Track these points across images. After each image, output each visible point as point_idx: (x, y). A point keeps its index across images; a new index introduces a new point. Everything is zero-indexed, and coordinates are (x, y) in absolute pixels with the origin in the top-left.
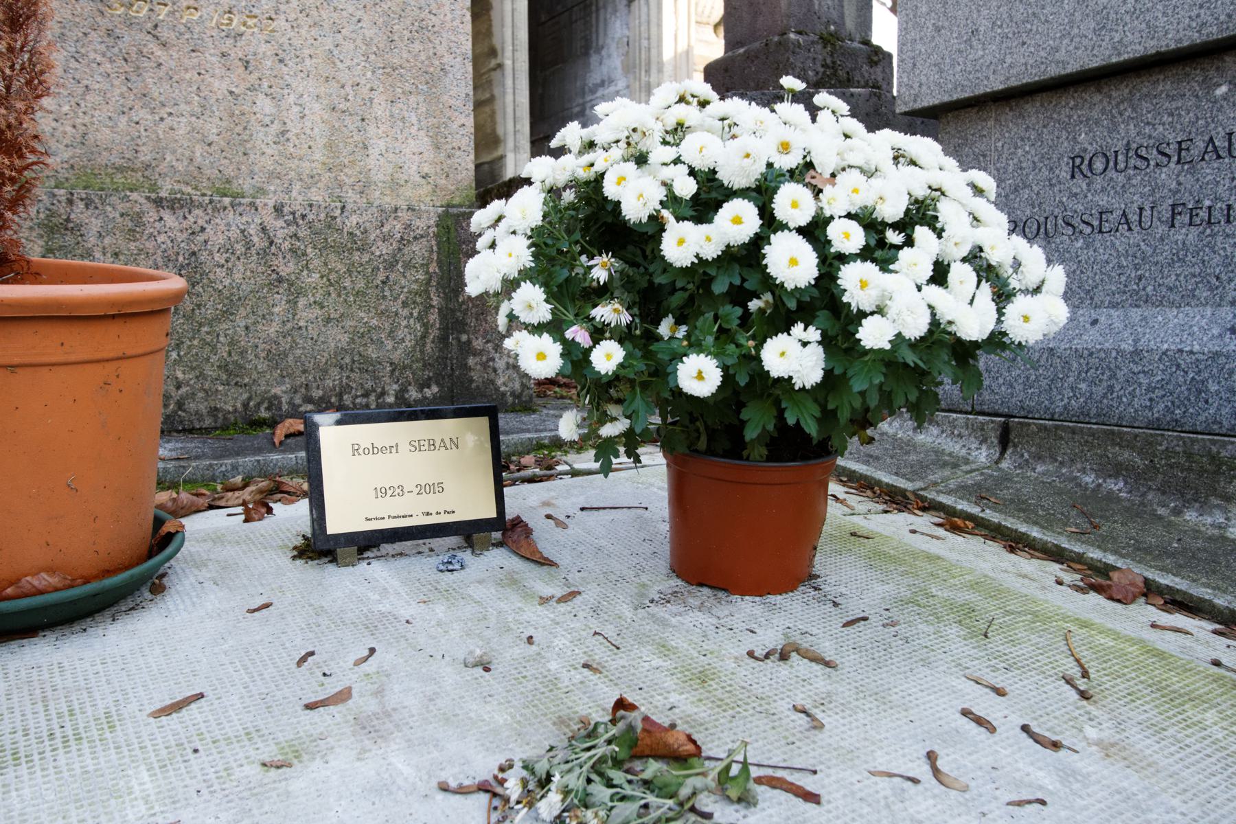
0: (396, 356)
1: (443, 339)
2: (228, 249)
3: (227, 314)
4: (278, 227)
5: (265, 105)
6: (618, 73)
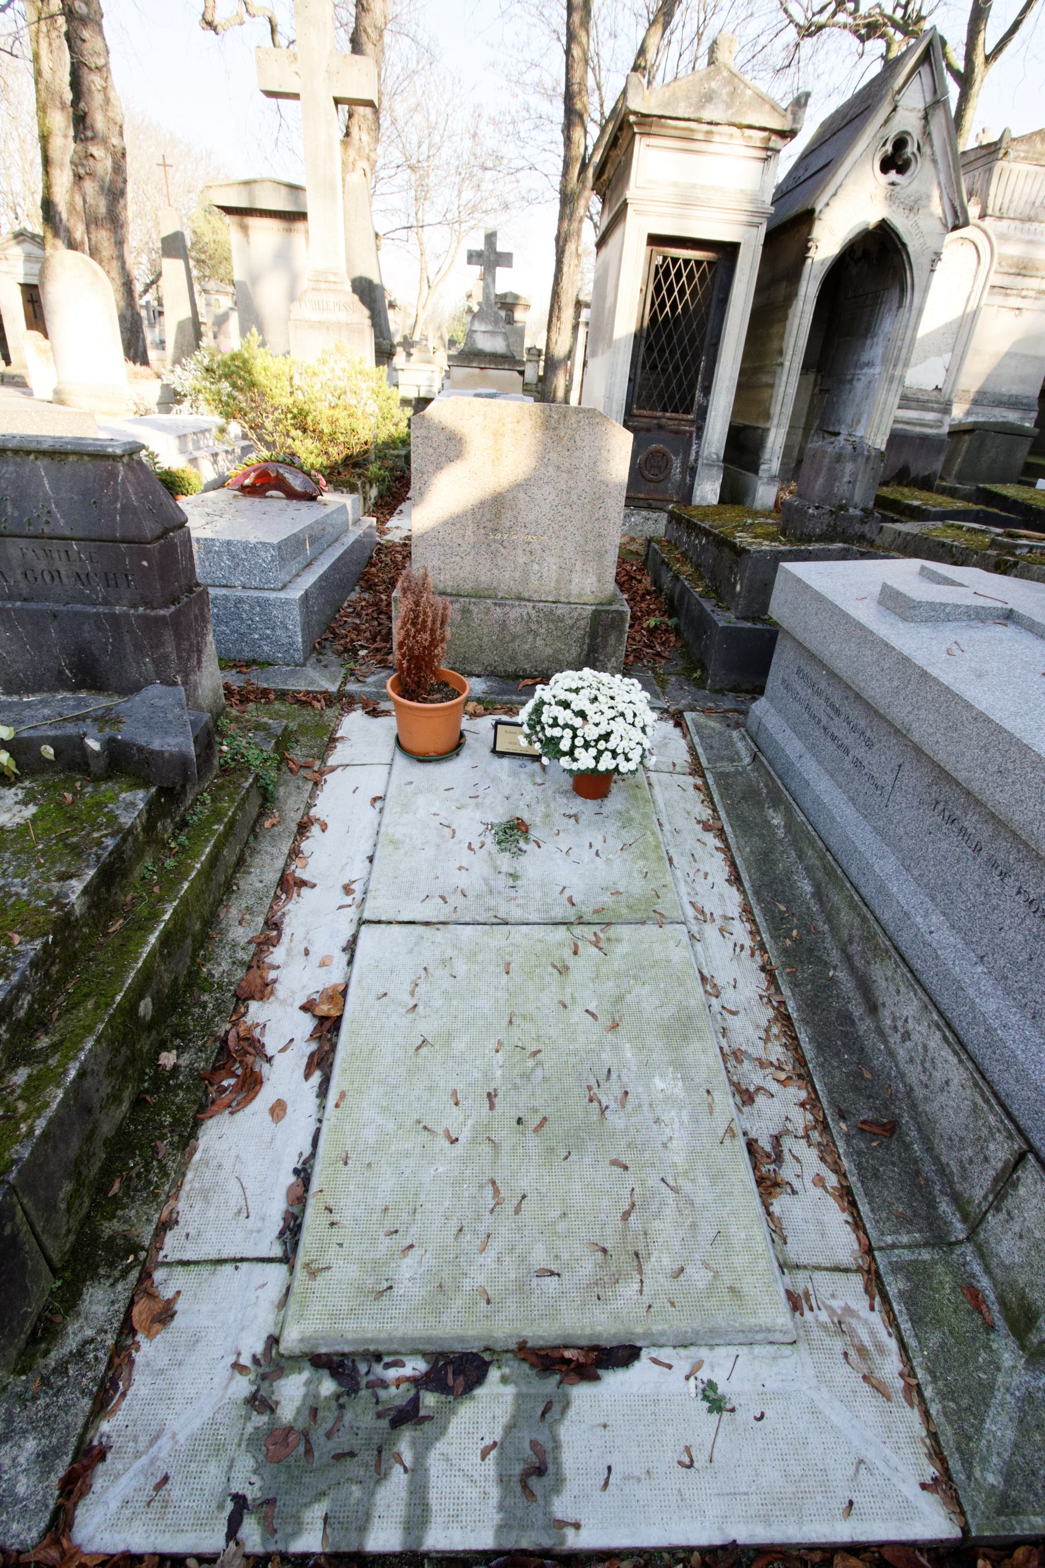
0: (570, 659)
1: (588, 655)
2: (516, 620)
3: (513, 641)
4: (533, 613)
5: (536, 567)
6: (878, 361)
